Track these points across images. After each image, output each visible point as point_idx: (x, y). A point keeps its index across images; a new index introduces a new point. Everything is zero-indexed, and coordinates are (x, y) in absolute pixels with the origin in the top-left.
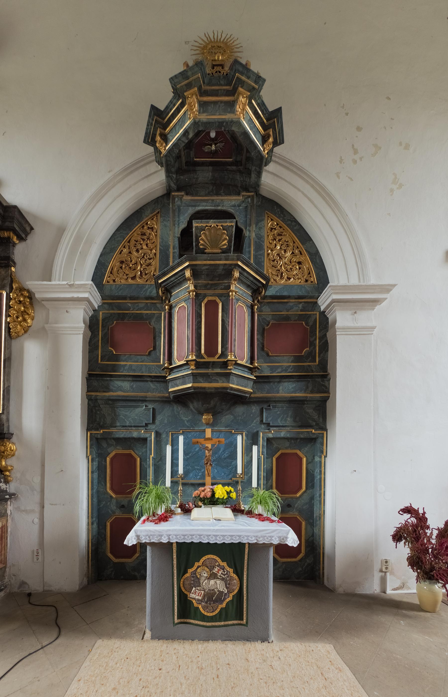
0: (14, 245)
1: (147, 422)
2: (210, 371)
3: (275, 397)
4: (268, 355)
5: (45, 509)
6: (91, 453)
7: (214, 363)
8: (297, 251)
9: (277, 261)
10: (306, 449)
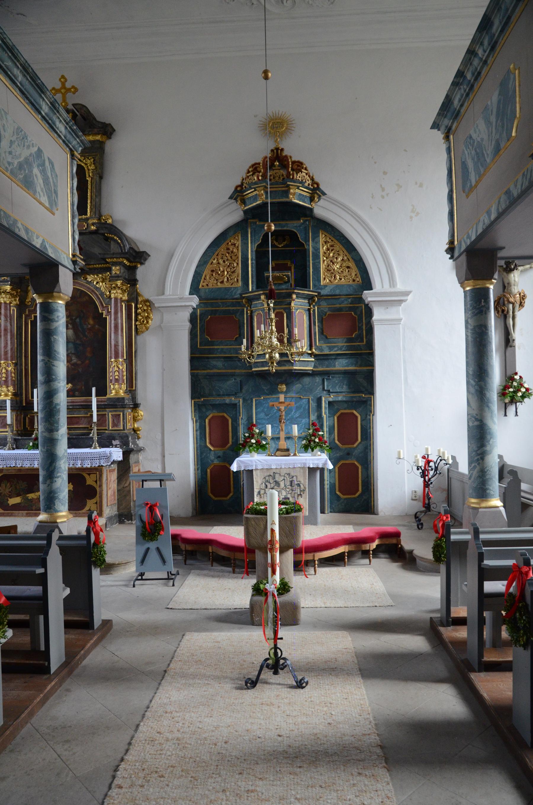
3: (332, 370)
4: (326, 338)
6: (195, 417)
8: (345, 258)
10: (361, 409)
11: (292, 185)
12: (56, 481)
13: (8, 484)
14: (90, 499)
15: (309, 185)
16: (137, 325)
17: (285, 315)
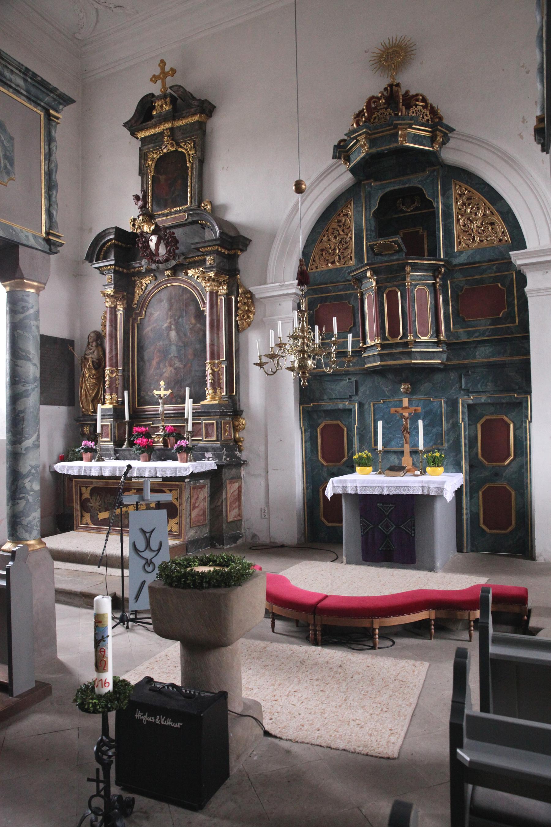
0: (239, 256)
1: (350, 394)
2: (394, 351)
4: (464, 320)
5: (269, 473)
6: (304, 425)
7: (397, 344)
8: (488, 212)
9: (468, 226)
10: (513, 414)
11: (401, 124)
12: (18, 504)
13: (98, 498)
14: (172, 519)
15: (428, 120)
16: (237, 321)
17: (399, 294)
